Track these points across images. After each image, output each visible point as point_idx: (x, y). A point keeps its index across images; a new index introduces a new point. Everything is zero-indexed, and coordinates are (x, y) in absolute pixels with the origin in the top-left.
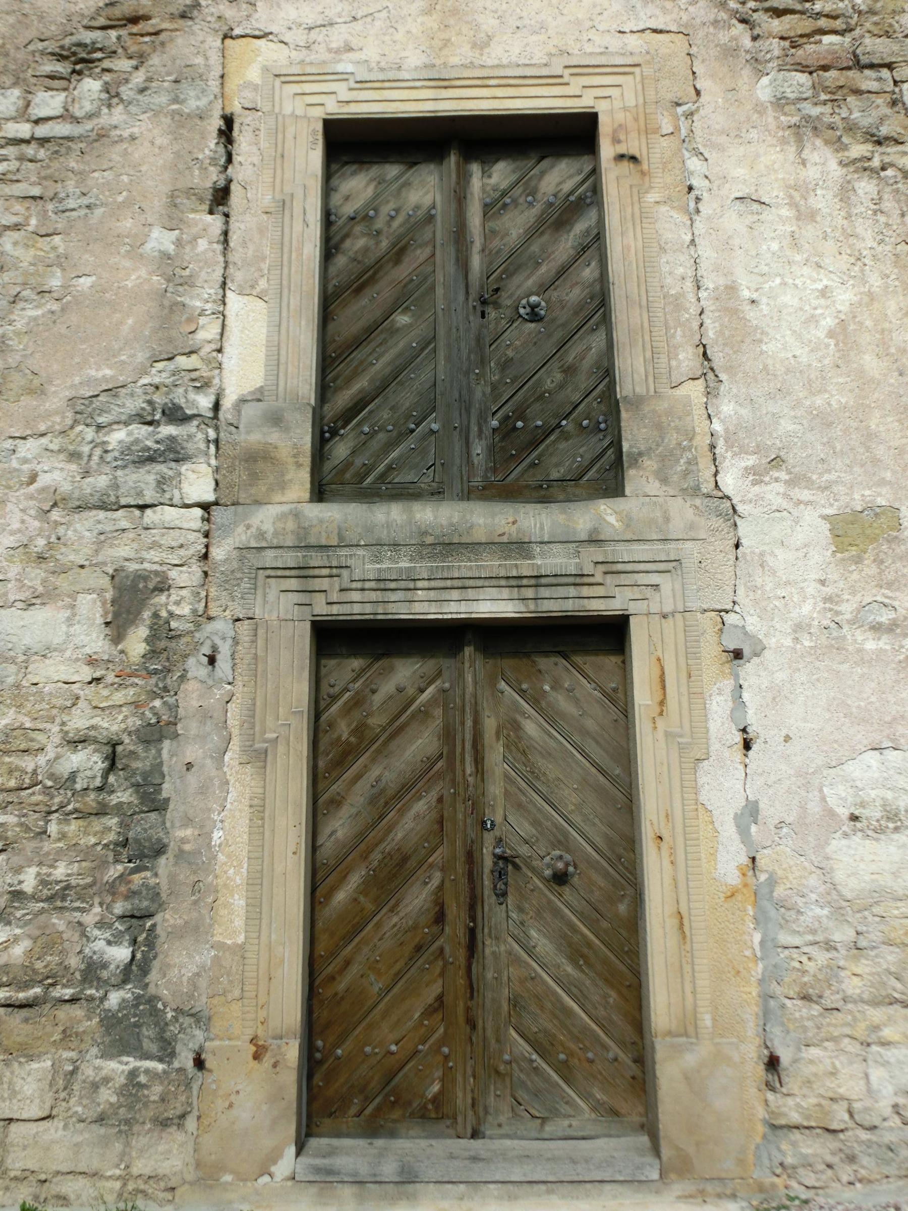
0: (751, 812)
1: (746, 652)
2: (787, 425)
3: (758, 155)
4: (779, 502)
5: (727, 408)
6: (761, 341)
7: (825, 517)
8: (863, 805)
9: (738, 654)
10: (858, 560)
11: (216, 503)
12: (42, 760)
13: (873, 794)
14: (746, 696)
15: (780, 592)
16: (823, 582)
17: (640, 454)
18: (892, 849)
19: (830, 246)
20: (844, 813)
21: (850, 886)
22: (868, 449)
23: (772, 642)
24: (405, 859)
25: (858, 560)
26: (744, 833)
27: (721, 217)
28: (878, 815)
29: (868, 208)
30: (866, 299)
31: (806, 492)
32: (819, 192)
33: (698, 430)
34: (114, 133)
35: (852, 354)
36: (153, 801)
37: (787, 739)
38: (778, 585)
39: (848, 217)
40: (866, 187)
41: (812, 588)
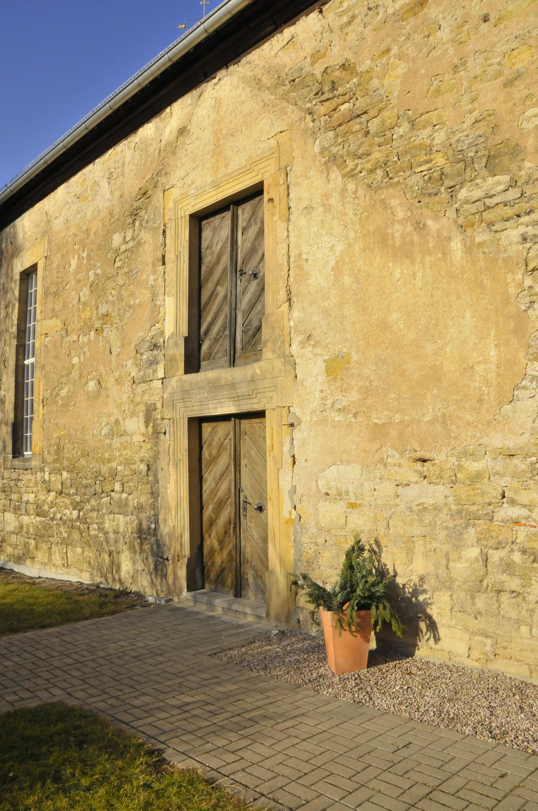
0: (294, 490)
1: (295, 424)
2: (315, 318)
3: (312, 183)
4: (310, 355)
5: (296, 314)
6: (308, 279)
7: (324, 361)
8: (329, 488)
9: (292, 425)
10: (335, 380)
11: (165, 378)
12: (136, 466)
13: (334, 484)
14: (294, 442)
15: (307, 397)
16: (322, 391)
17: (267, 341)
18: (338, 508)
19: (336, 222)
20: (323, 491)
21: (324, 522)
22: (342, 324)
23: (303, 419)
24: (221, 501)
25: (335, 380)
26: (292, 499)
27: (299, 220)
28: (335, 493)
29: (351, 197)
30: (348, 247)
31: (319, 349)
32: (333, 195)
33: (285, 326)
34: (143, 241)
35: (340, 277)
36: (157, 481)
37: (306, 460)
38: (306, 394)
39: (343, 205)
40: (351, 186)
41: (318, 394)
